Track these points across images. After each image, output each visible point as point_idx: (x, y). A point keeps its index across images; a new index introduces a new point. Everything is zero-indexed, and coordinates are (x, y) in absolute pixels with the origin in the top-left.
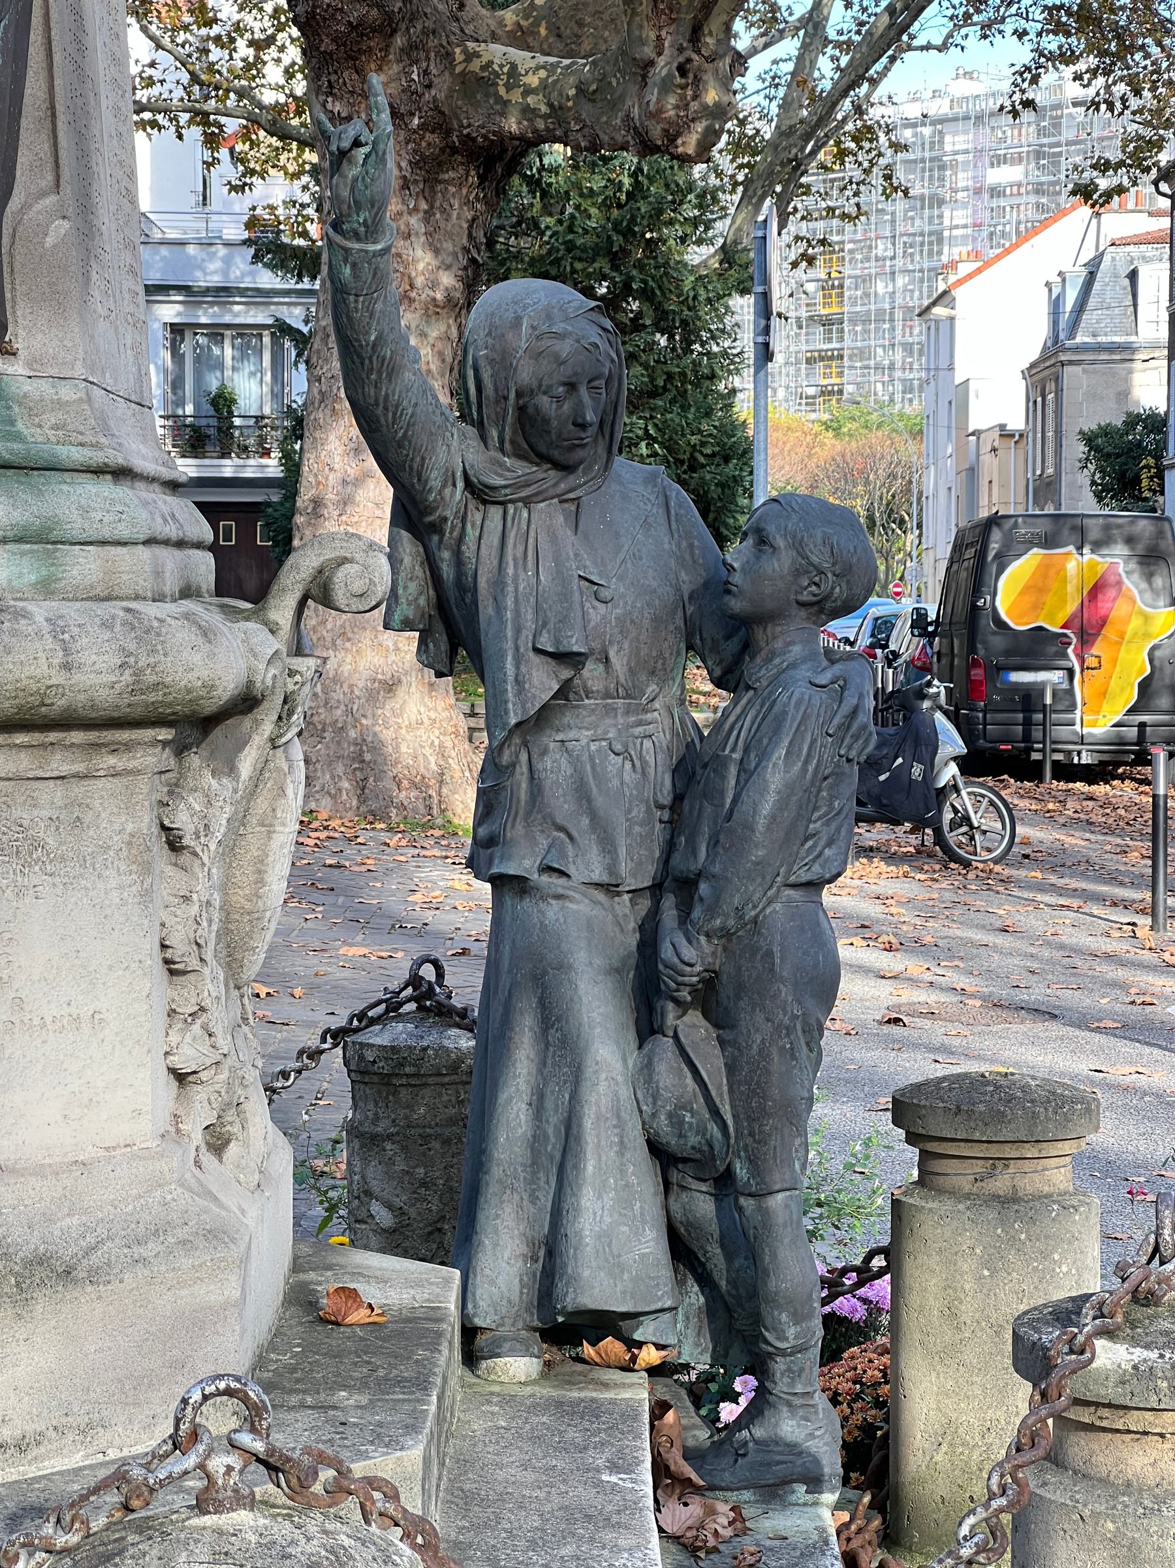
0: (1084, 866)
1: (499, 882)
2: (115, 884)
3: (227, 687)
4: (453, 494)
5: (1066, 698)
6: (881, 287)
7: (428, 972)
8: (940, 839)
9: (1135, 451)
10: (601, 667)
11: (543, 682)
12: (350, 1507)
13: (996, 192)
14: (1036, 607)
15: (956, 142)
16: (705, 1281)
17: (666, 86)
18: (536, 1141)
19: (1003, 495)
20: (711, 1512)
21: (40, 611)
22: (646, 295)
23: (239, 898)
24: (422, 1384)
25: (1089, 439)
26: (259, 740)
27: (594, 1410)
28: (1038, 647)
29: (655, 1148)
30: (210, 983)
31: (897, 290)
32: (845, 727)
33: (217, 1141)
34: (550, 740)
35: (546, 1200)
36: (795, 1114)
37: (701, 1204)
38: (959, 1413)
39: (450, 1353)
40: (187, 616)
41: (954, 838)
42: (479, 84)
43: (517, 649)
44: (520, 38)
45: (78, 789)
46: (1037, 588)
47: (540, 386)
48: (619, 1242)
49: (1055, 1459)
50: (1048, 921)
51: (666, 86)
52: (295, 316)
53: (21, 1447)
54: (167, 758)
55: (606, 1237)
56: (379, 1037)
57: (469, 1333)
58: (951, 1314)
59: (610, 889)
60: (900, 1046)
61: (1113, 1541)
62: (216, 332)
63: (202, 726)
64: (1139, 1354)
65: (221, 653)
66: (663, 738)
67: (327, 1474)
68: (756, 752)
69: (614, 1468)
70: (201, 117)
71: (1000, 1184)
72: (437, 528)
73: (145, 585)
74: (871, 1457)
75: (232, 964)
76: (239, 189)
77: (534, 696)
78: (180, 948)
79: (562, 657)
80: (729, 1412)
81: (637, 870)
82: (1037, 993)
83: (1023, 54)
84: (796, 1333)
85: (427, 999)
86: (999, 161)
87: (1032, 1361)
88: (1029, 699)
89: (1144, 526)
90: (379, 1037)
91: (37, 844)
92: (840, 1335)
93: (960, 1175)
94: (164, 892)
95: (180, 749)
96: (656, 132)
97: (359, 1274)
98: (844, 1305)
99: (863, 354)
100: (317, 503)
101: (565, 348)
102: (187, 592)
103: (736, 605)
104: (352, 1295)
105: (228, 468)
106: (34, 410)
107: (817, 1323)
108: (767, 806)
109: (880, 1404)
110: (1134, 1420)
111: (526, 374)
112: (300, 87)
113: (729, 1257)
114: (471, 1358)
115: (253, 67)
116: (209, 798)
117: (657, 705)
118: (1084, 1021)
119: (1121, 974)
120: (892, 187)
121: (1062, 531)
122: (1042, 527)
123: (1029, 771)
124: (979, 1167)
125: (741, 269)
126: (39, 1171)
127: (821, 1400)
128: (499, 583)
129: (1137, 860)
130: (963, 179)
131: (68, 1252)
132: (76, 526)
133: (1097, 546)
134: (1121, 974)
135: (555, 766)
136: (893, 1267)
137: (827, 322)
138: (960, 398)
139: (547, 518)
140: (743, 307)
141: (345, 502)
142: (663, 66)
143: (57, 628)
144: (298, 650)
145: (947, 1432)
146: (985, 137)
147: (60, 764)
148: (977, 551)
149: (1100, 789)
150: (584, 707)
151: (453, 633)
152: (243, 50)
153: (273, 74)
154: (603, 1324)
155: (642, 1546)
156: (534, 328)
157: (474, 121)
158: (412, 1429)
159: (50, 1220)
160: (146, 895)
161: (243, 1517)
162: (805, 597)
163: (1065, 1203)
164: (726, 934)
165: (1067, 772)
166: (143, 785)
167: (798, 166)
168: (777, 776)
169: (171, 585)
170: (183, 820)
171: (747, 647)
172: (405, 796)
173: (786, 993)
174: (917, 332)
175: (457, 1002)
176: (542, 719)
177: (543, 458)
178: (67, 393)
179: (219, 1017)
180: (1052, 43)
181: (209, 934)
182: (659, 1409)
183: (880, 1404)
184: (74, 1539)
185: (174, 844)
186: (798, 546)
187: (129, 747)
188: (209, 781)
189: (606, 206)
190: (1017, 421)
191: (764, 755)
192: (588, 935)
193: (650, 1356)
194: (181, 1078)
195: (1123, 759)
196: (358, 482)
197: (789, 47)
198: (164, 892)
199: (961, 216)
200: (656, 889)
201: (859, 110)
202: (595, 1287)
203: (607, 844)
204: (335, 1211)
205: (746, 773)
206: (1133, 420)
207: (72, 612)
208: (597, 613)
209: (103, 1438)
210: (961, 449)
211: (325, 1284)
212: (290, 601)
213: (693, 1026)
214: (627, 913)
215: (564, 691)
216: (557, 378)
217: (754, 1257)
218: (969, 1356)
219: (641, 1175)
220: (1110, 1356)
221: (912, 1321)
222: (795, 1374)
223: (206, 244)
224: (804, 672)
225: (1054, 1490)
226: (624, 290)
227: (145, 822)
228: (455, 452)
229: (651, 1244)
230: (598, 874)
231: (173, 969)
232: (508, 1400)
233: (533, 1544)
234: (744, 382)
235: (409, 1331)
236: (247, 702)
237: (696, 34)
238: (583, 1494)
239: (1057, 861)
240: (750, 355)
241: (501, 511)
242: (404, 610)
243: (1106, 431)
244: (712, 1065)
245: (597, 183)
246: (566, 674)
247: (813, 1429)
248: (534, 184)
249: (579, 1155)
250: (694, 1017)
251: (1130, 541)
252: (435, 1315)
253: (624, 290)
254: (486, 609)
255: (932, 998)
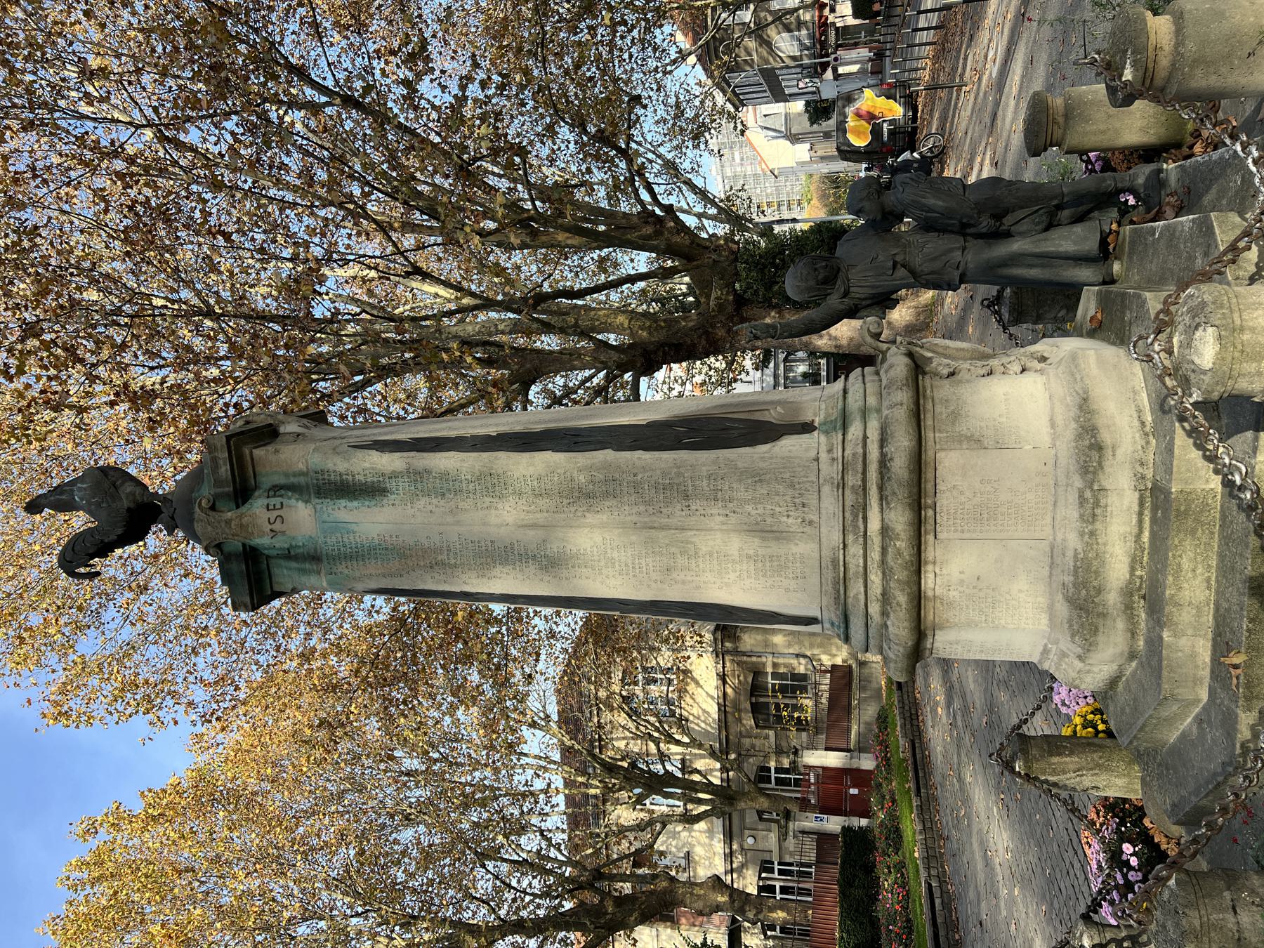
0: (945, 111)
1: (961, 282)
2: (965, 392)
3: (906, 360)
5: (892, 122)
6: (769, 191)
7: (986, 303)
8: (936, 156)
9: (816, 109)
11: (901, 272)
12: (1173, 309)
13: (742, 159)
14: (864, 133)
15: (729, 172)
16: (1090, 211)
17: (720, 255)
18: (1043, 266)
19: (830, 148)
20: (1168, 203)
21: (885, 412)
22: (774, 258)
23: (968, 355)
24: (1125, 294)
25: (812, 124)
26: (922, 351)
27: (1132, 242)
28: (876, 132)
29: (1047, 229)
30: (994, 363)
31: (770, 184)
32: (916, 181)
33: (1043, 359)
34: (918, 269)
35: (1062, 261)
36: (1035, 186)
37: (1065, 214)
38: (1137, 124)
39: (1113, 288)
40: (886, 372)
41: (936, 151)
42: (721, 307)
44: (708, 297)
45: (937, 401)
46: (858, 133)
48: (1074, 239)
49: (1163, 89)
50: (964, 117)
51: (720, 255)
52: (782, 356)
53: (1140, 411)
54: (927, 377)
55: (1075, 243)
56: (1006, 316)
57: (1104, 283)
58: (1103, 132)
59: (964, 249)
60: (1004, 162)
61: (1192, 67)
62: (786, 378)
63: (918, 368)
64: (1127, 66)
65: (897, 364)
66: (918, 236)
67: (1161, 316)
68: (922, 207)
69: (1154, 234)
70: (730, 384)
71: (1061, 120)
72: (856, 306)
73: (877, 384)
74: (1149, 153)
75: (988, 357)
76: (748, 373)
78: (984, 371)
79: (894, 267)
80: (1132, 202)
81: (957, 241)
82: (988, 120)
83: (706, 154)
84: (1109, 181)
85: (992, 304)
86: (733, 159)
87: (1128, 101)
88: (891, 132)
89: (840, 103)
90: (1006, 316)
91: (953, 412)
92: (1107, 167)
93: (1058, 133)
94: (967, 377)
95: (924, 373)
96: (732, 257)
97: (1084, 317)
98: (1097, 167)
99: (788, 194)
100: (836, 347)
101: (805, 272)
102: (877, 373)
103: (879, 217)
104: (1092, 319)
105: (824, 373)
106: (828, 415)
107: (1106, 174)
108: (941, 203)
109: (1132, 154)
110: (1150, 65)
111: (812, 283)
112: (720, 357)
113: (1082, 204)
114: (1113, 282)
115: (716, 370)
116: (941, 365)
118: (997, 104)
119: (981, 94)
120: (742, 189)
121: (841, 128)
122: (840, 134)
123: (915, 130)
124: (1055, 128)
125: (766, 230)
126: (1052, 409)
127: (1131, 172)
128: (872, 287)
129: (942, 94)
130: (739, 169)
131: (1078, 400)
132: (860, 403)
133: (846, 117)
134: (981, 94)
135: (927, 267)
136: (1086, 152)
137: (779, 206)
138: (802, 164)
139: (854, 275)
140: (777, 229)
141: (835, 338)
142: (714, 257)
143: (890, 407)
144: (894, 342)
145: (1144, 130)
146: (727, 164)
147: (929, 406)
148: (848, 153)
149: (920, 108)
151: (885, 301)
152: (712, 373)
153: (717, 365)
154: (1104, 243)
155: (1181, 222)
157: (730, 309)
158: (1139, 296)
159: (1067, 405)
160: (968, 381)
161: (1175, 340)
163: (1068, 98)
164: (979, 213)
165: (914, 119)
166: (935, 383)
167: (738, 217)
168: (932, 201)
169: (876, 378)
170: (945, 372)
171: (891, 213)
172: (922, 318)
173: (998, 193)
174: (782, 178)
175: (995, 293)
176: (913, 273)
177: (836, 277)
178: (823, 406)
179: (1005, 360)
180: (702, 146)
181: (979, 363)
182: (1132, 222)
183: (1132, 154)
184: (1179, 390)
185: (952, 374)
186: (861, 200)
187: (924, 387)
188: (933, 365)
189: (750, 271)
190: (808, 146)
191: (925, 205)
192: (975, 255)
193: (1114, 226)
194: (1023, 370)
195: (910, 102)
196: (830, 335)
197: (705, 222)
198: (967, 377)
199: (749, 168)
200: (965, 235)
201: (722, 201)
202: (1092, 245)
203: (951, 250)
204: (1062, 328)
205: (930, 210)
206: (807, 111)
207: (885, 404)
208: (881, 258)
209: (1137, 388)
210: (816, 162)
211: (1088, 326)
212: (880, 344)
213: (1008, 220)
214: (972, 243)
215: (904, 266)
217: (1083, 196)
218: (1118, 125)
219: (1055, 234)
220: (1128, 75)
221: (1106, 144)
222: (1123, 180)
223: (762, 381)
224: (899, 196)
225: (1173, 89)
226: (773, 264)
227: (946, 382)
228: (834, 301)
229: (1078, 229)
230: (959, 253)
231: (991, 373)
232: (1128, 269)
233: (1179, 257)
234: (798, 227)
235: (1105, 302)
236: (910, 355)
237: (707, 248)
238: (1162, 244)
239: (943, 120)
240: (791, 225)
242: (880, 313)
243: (810, 119)
244: (1020, 214)
245: (744, 274)
247: (1142, 173)
248: (745, 292)
249: (1048, 252)
250: (1005, 221)
251: (844, 107)
252: (1100, 293)
253: (773, 264)
254: (880, 290)
255: (989, 153)
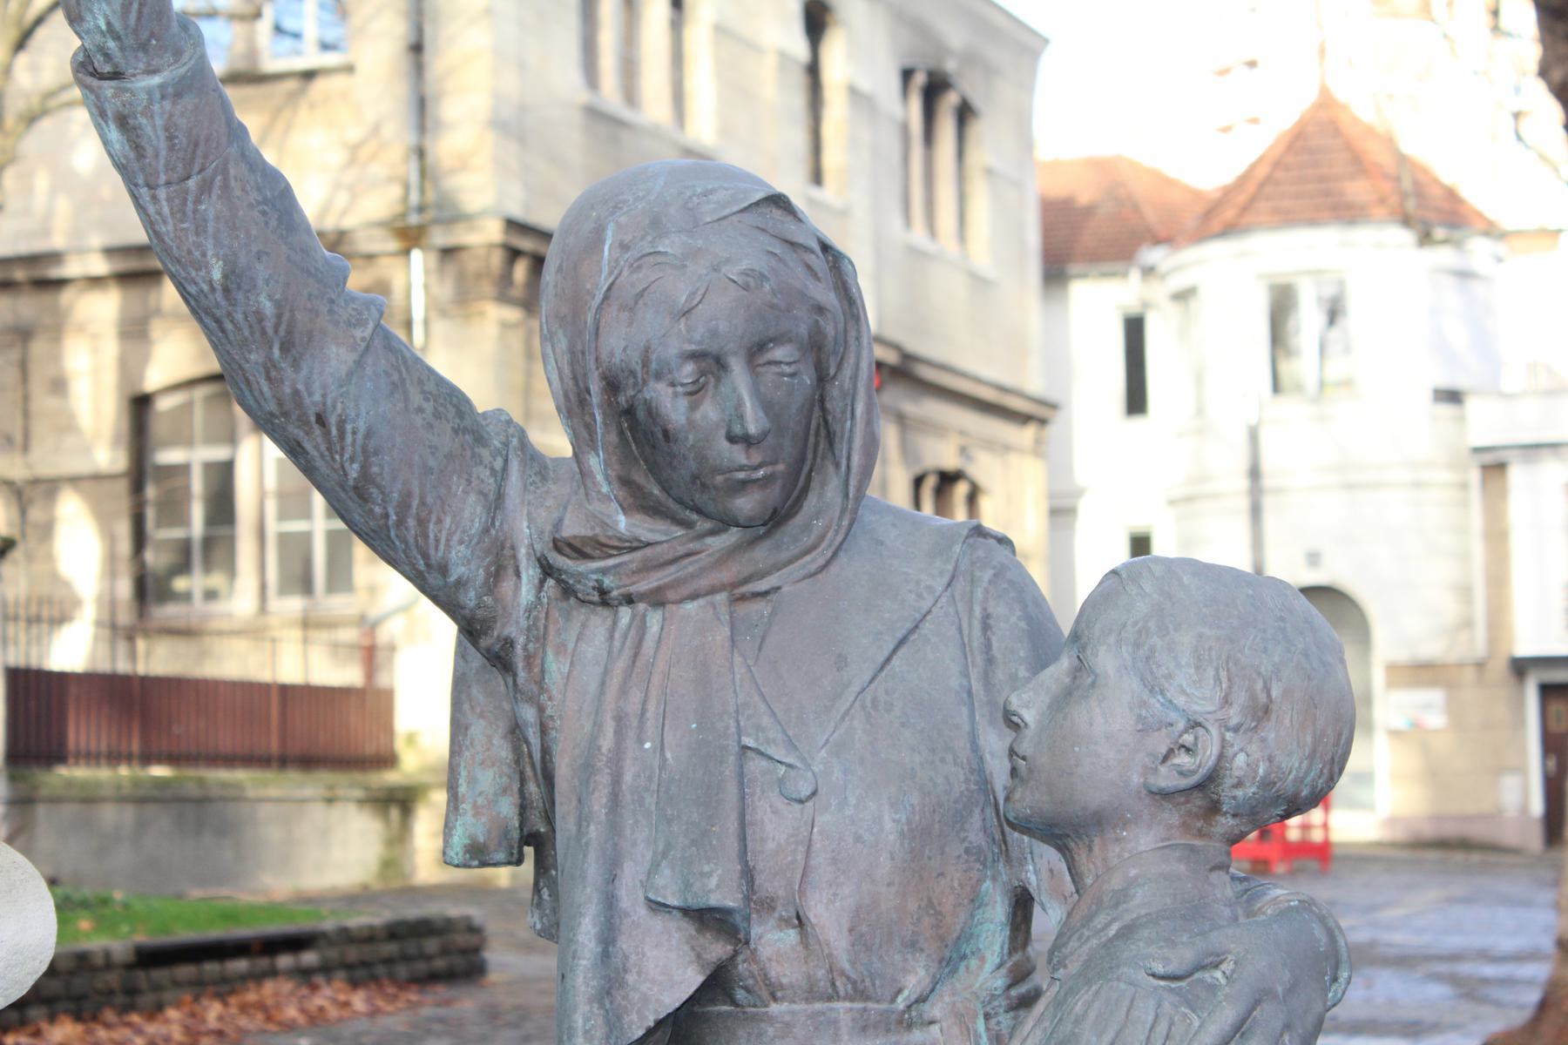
4: (517, 588)
10: (792, 935)
40: (1194, 772)
43: (610, 902)
47: (645, 364)
77: (645, 999)
79: (707, 918)
117: (935, 1009)
150: (770, 1019)
156: (624, 247)
162: (1166, 779)
216: (673, 349)
241: (609, 621)
246: (718, 950)
